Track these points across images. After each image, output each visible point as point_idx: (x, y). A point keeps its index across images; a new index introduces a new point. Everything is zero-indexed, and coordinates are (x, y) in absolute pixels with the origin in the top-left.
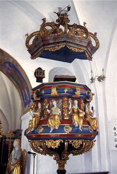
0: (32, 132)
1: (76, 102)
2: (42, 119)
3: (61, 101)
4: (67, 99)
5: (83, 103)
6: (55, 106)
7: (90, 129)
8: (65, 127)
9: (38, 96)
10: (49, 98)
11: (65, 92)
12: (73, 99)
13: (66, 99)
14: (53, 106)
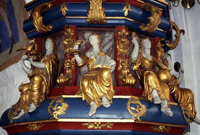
0: (28, 115)
1: (147, 43)
2: (62, 80)
3: (109, 36)
4: (127, 33)
5: (163, 50)
6: (96, 48)
7: (185, 114)
8: (129, 103)
9: (45, 22)
10: (79, 29)
11: (126, 13)
12: (142, 35)
13: (124, 31)
14: (89, 47)
